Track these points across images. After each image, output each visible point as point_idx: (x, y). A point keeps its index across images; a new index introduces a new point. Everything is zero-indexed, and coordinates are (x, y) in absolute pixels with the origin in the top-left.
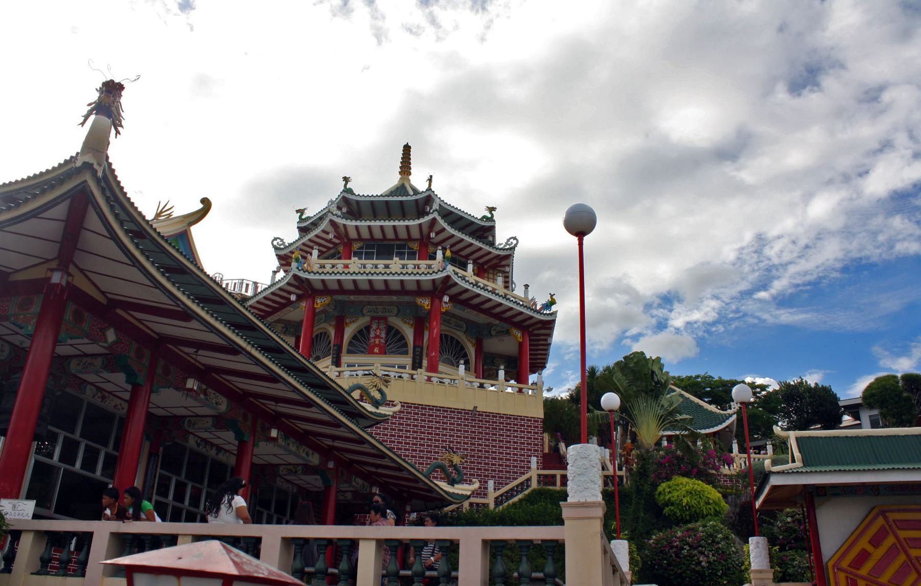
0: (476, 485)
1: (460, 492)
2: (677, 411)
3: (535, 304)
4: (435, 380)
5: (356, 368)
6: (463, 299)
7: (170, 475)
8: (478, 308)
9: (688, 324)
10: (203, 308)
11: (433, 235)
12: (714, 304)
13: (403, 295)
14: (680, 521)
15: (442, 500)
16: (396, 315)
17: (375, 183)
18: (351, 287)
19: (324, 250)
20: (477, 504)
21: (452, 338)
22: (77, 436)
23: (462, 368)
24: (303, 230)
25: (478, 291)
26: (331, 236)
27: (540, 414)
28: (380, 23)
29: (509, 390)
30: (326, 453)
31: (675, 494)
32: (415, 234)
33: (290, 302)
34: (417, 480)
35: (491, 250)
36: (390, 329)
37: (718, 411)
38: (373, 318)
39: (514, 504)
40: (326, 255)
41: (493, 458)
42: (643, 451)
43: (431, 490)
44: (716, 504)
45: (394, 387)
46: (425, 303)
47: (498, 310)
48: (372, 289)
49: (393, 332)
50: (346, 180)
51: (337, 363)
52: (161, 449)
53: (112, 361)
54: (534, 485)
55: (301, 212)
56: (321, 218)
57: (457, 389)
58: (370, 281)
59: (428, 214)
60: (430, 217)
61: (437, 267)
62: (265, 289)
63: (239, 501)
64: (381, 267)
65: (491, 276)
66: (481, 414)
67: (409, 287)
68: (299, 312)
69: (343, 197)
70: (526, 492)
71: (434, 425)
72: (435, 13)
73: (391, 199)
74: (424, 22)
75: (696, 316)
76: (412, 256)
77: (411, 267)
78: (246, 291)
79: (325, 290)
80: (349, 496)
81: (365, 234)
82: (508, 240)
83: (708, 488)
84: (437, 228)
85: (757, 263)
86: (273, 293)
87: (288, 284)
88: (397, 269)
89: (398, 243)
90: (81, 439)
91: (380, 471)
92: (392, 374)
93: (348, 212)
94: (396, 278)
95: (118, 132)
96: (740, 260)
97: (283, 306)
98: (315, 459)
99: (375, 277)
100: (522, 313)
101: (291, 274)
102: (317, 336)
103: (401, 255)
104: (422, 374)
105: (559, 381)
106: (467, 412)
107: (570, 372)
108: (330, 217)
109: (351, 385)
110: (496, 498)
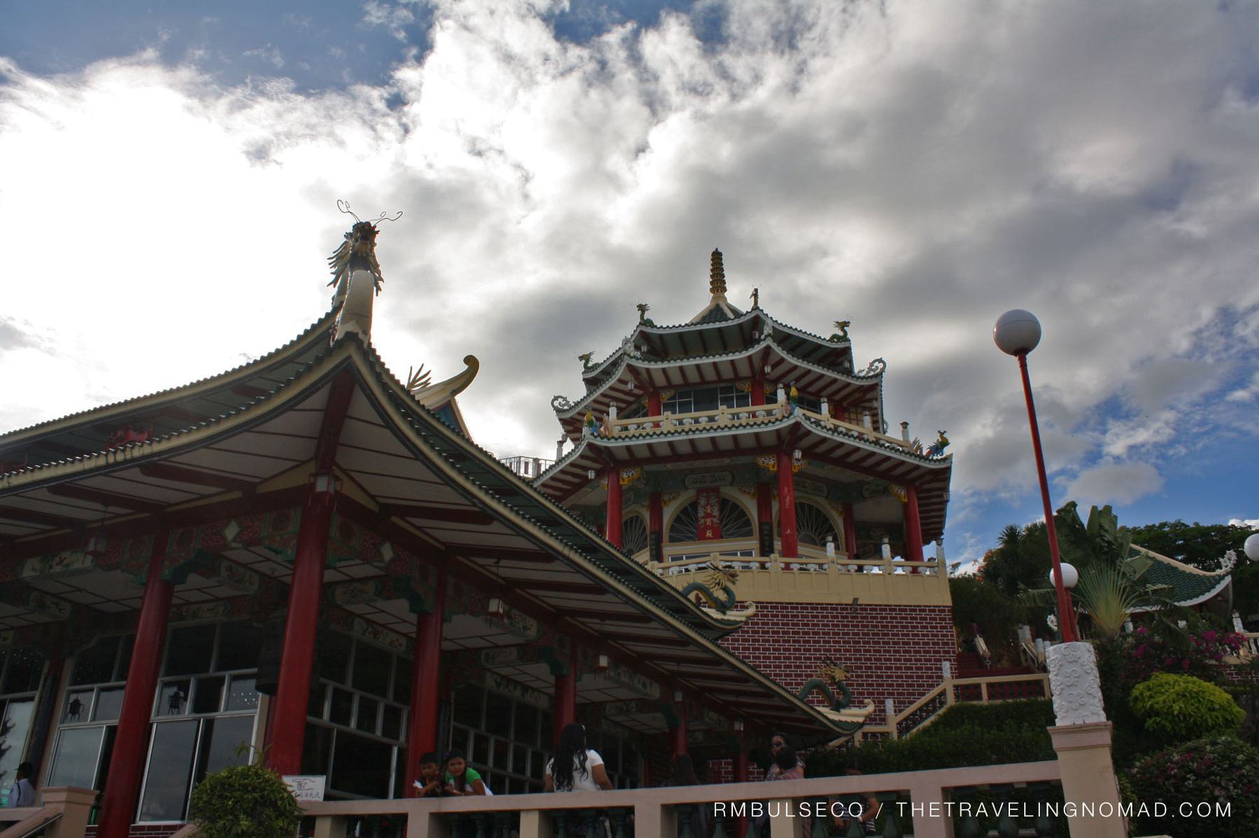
0: (871, 708)
1: (849, 719)
2: (1144, 581)
3: (920, 448)
4: (795, 567)
5: (684, 561)
6: (821, 452)
7: (130, 677)
8: (842, 462)
9: (1132, 448)
10: (505, 505)
11: (768, 369)
12: (1169, 416)
13: (737, 455)
14: (1173, 738)
15: (828, 732)
16: (731, 484)
17: (681, 311)
18: (666, 451)
19: (623, 405)
20: (874, 734)
21: (810, 507)
22: (348, 686)
23: (831, 546)
24: (592, 383)
25: (840, 439)
26: (630, 386)
27: (947, 600)
28: (651, 86)
29: (900, 571)
30: (668, 681)
31: (1160, 699)
32: (744, 371)
33: (586, 480)
34: (793, 708)
35: (849, 380)
36: (724, 503)
37: (1202, 573)
38: (699, 491)
39: (926, 730)
40: (626, 412)
41: (887, 668)
42: (1104, 640)
43: (813, 720)
44: (1225, 710)
45: (750, 582)
46: (770, 463)
47: (839, 453)
48: (695, 452)
49: (683, 517)
50: (642, 308)
51: (658, 556)
52: (453, 695)
53: (388, 586)
54: (951, 700)
55: (586, 358)
56: (615, 364)
57: (825, 577)
58: (692, 441)
59: (758, 341)
60: (763, 345)
61: (778, 413)
62: (551, 467)
63: (594, 758)
64: (703, 420)
65: (853, 416)
66: (864, 608)
67: (746, 444)
68: (599, 493)
69: (642, 333)
70: (941, 712)
71: (801, 629)
72: (726, 63)
73: (705, 327)
74: (711, 78)
75: (1142, 436)
76: (742, 401)
77: (744, 416)
78: (526, 472)
79: (632, 459)
80: (700, 737)
81: (677, 379)
82: (872, 364)
83: (1210, 686)
84: (773, 359)
85: (1226, 349)
86: (562, 471)
87: (582, 456)
88: (725, 421)
89: (723, 385)
90: (353, 690)
91: (742, 699)
92: (737, 566)
93: (649, 352)
94: (727, 433)
95: (379, 289)
96: (1198, 348)
97: (576, 487)
98: (655, 692)
99: (697, 436)
100: (903, 463)
101: (584, 444)
102: (626, 522)
103: (728, 402)
104: (776, 561)
105: (964, 554)
106: (844, 607)
107: (968, 535)
108: (627, 360)
109: (685, 585)
110: (899, 724)
